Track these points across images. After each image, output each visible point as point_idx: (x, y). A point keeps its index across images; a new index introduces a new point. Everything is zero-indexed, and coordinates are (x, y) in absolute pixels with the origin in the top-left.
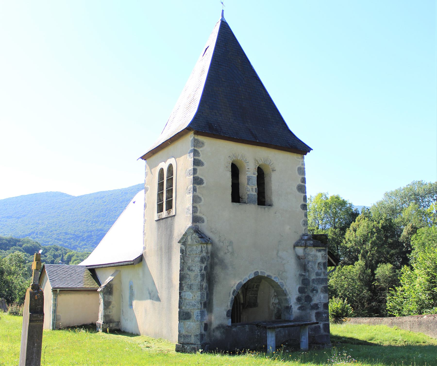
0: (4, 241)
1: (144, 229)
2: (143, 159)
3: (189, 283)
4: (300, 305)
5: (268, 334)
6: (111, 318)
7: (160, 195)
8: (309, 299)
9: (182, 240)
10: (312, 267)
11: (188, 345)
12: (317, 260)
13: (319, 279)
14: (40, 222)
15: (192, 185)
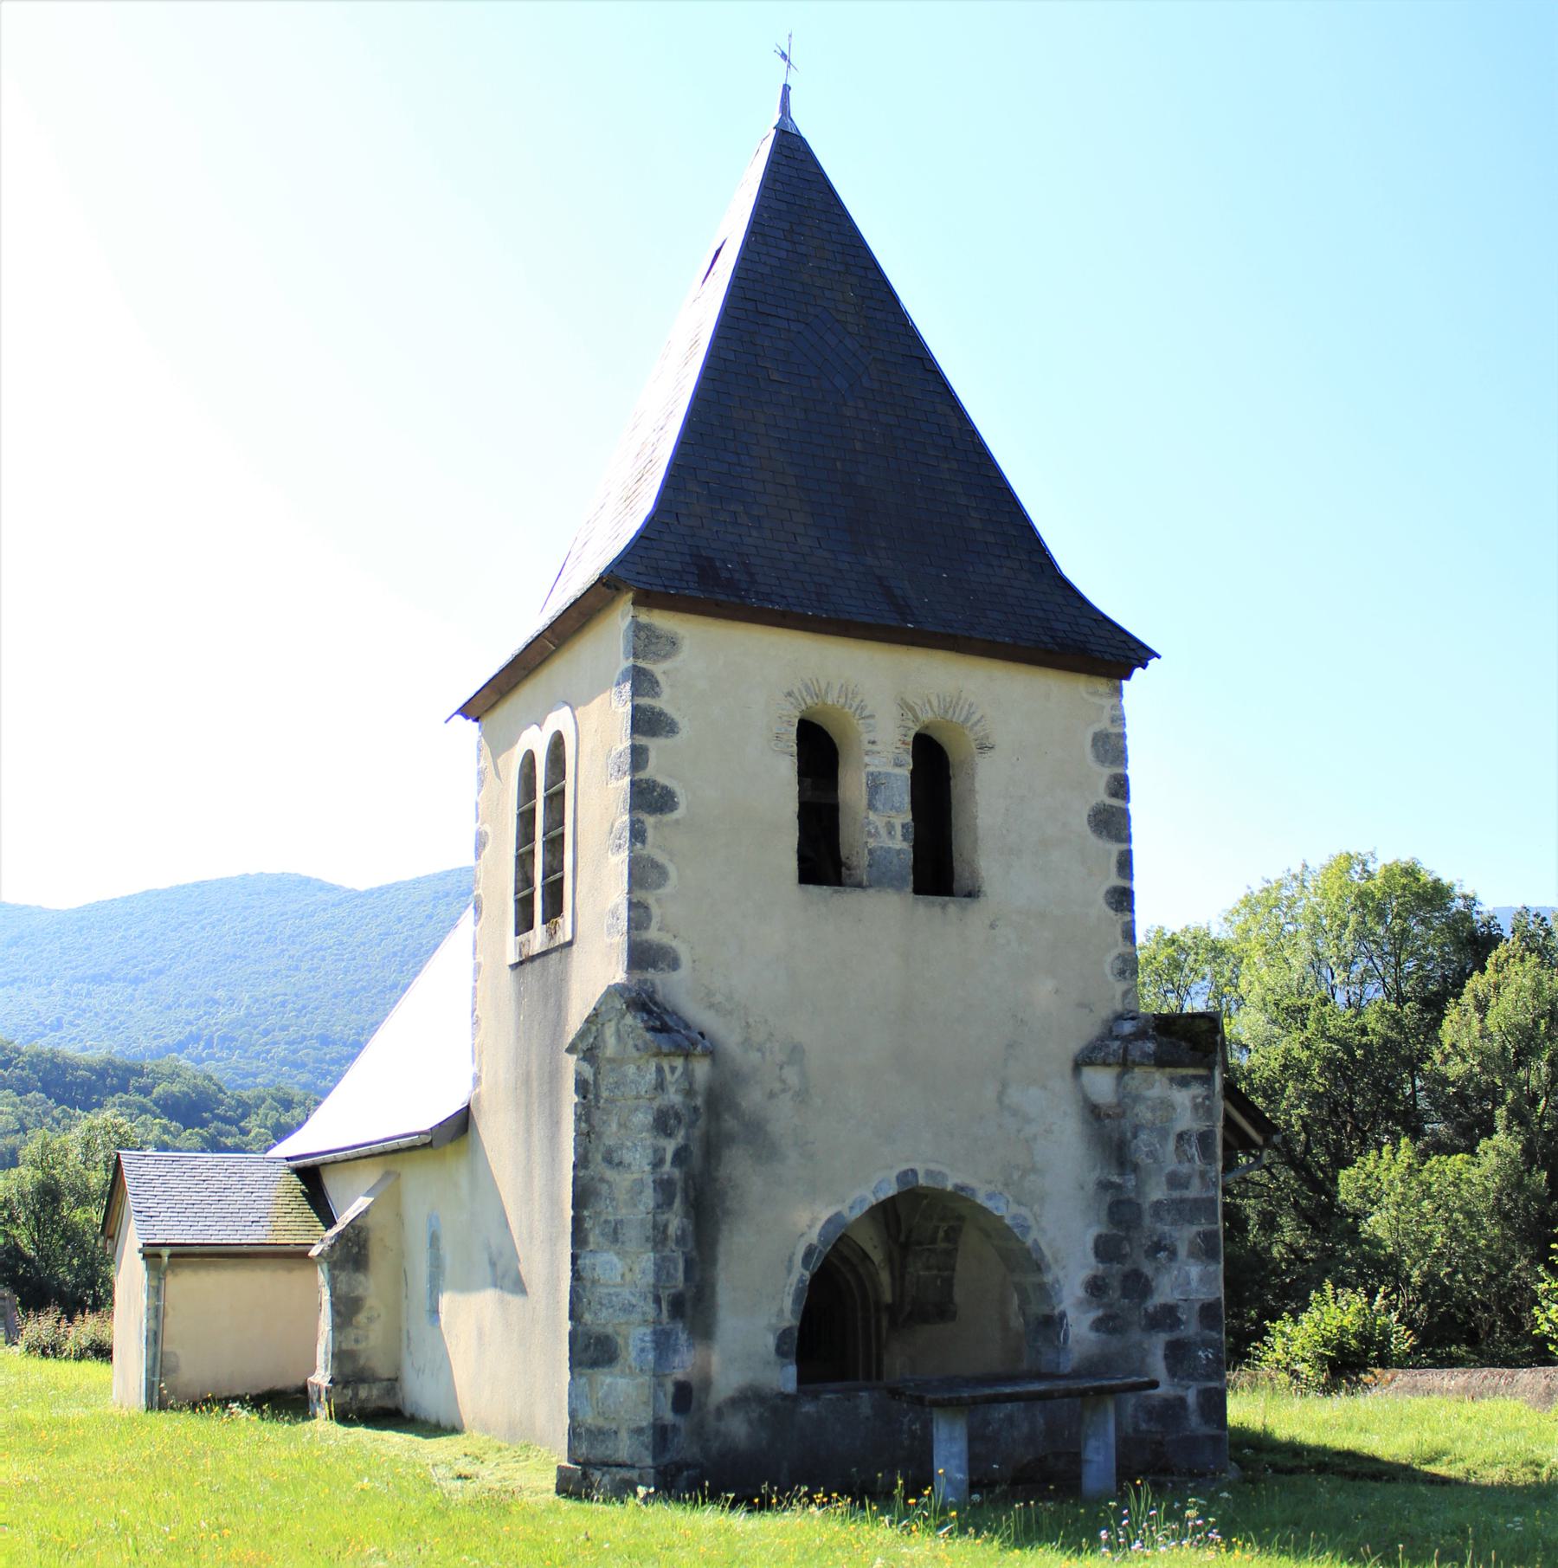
0: (81, 1073)
1: (474, 1003)
2: (467, 718)
3: (611, 1218)
4: (1100, 1313)
5: (937, 1428)
6: (362, 1362)
7: (524, 861)
8: (1138, 1285)
9: (581, 1042)
10: (1151, 1151)
11: (605, 1469)
12: (1170, 1120)
13: (1182, 1201)
14: (220, 994)
15: (628, 816)
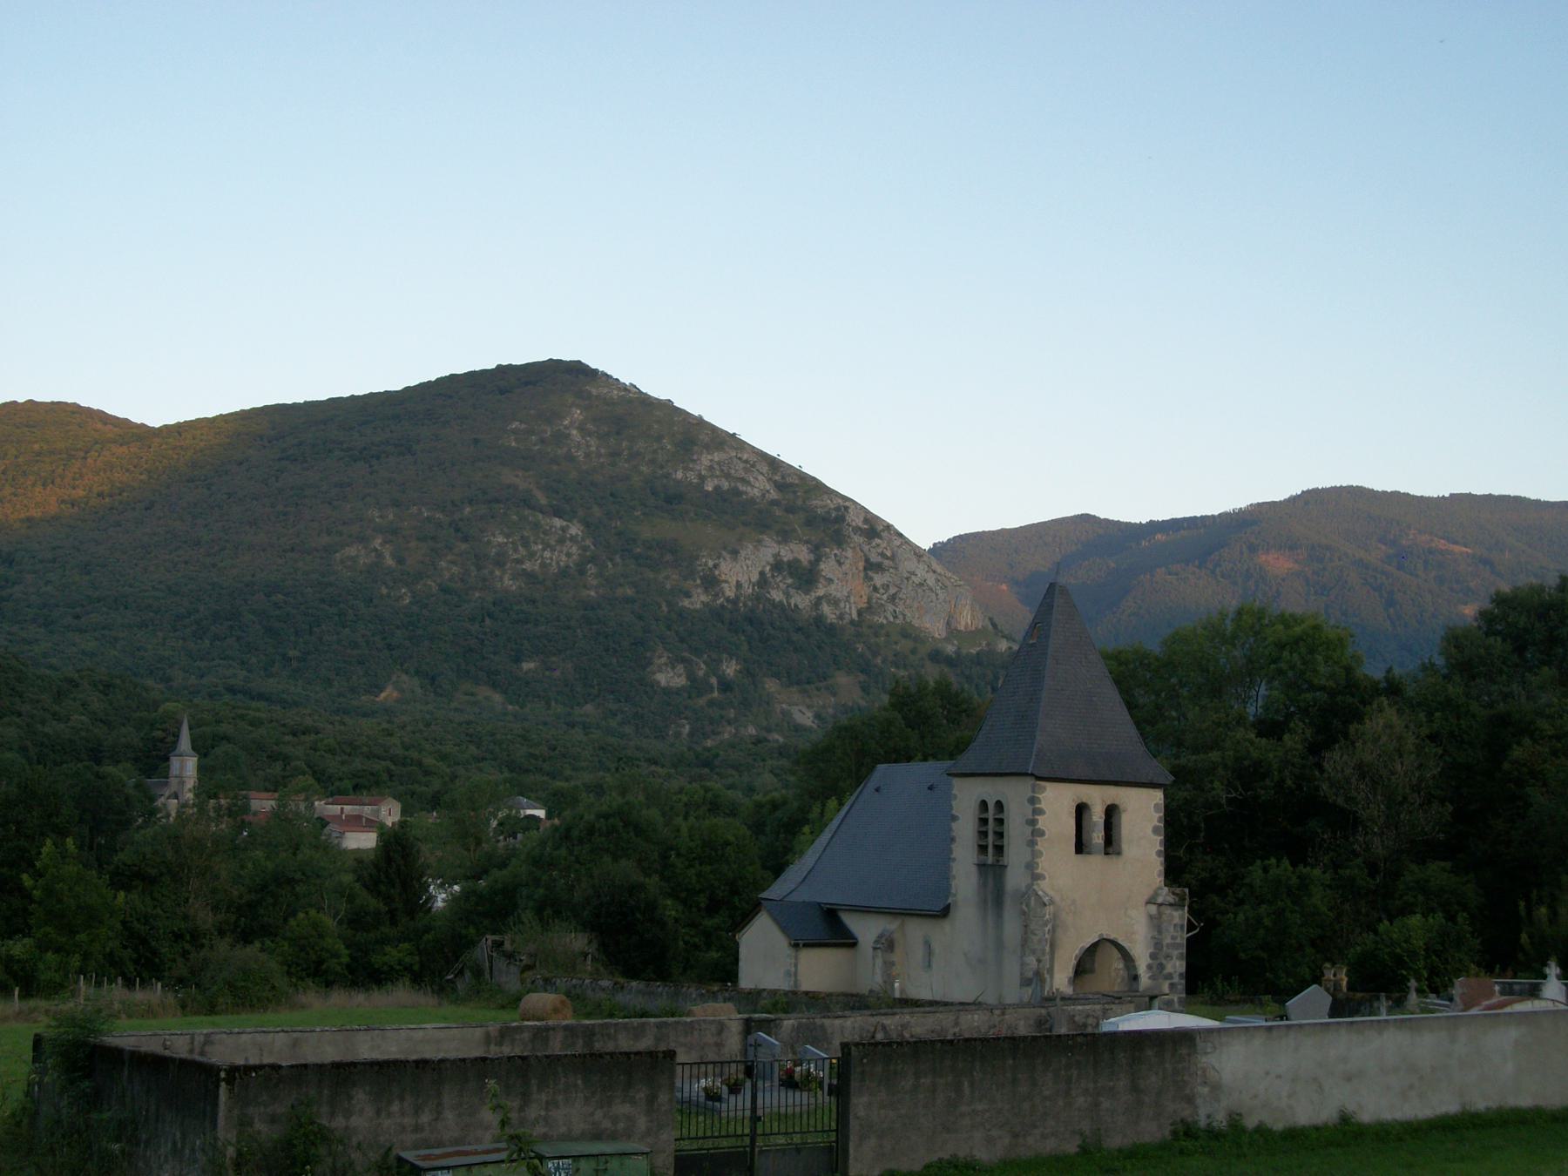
8: (1161, 967)
13: (1175, 943)
